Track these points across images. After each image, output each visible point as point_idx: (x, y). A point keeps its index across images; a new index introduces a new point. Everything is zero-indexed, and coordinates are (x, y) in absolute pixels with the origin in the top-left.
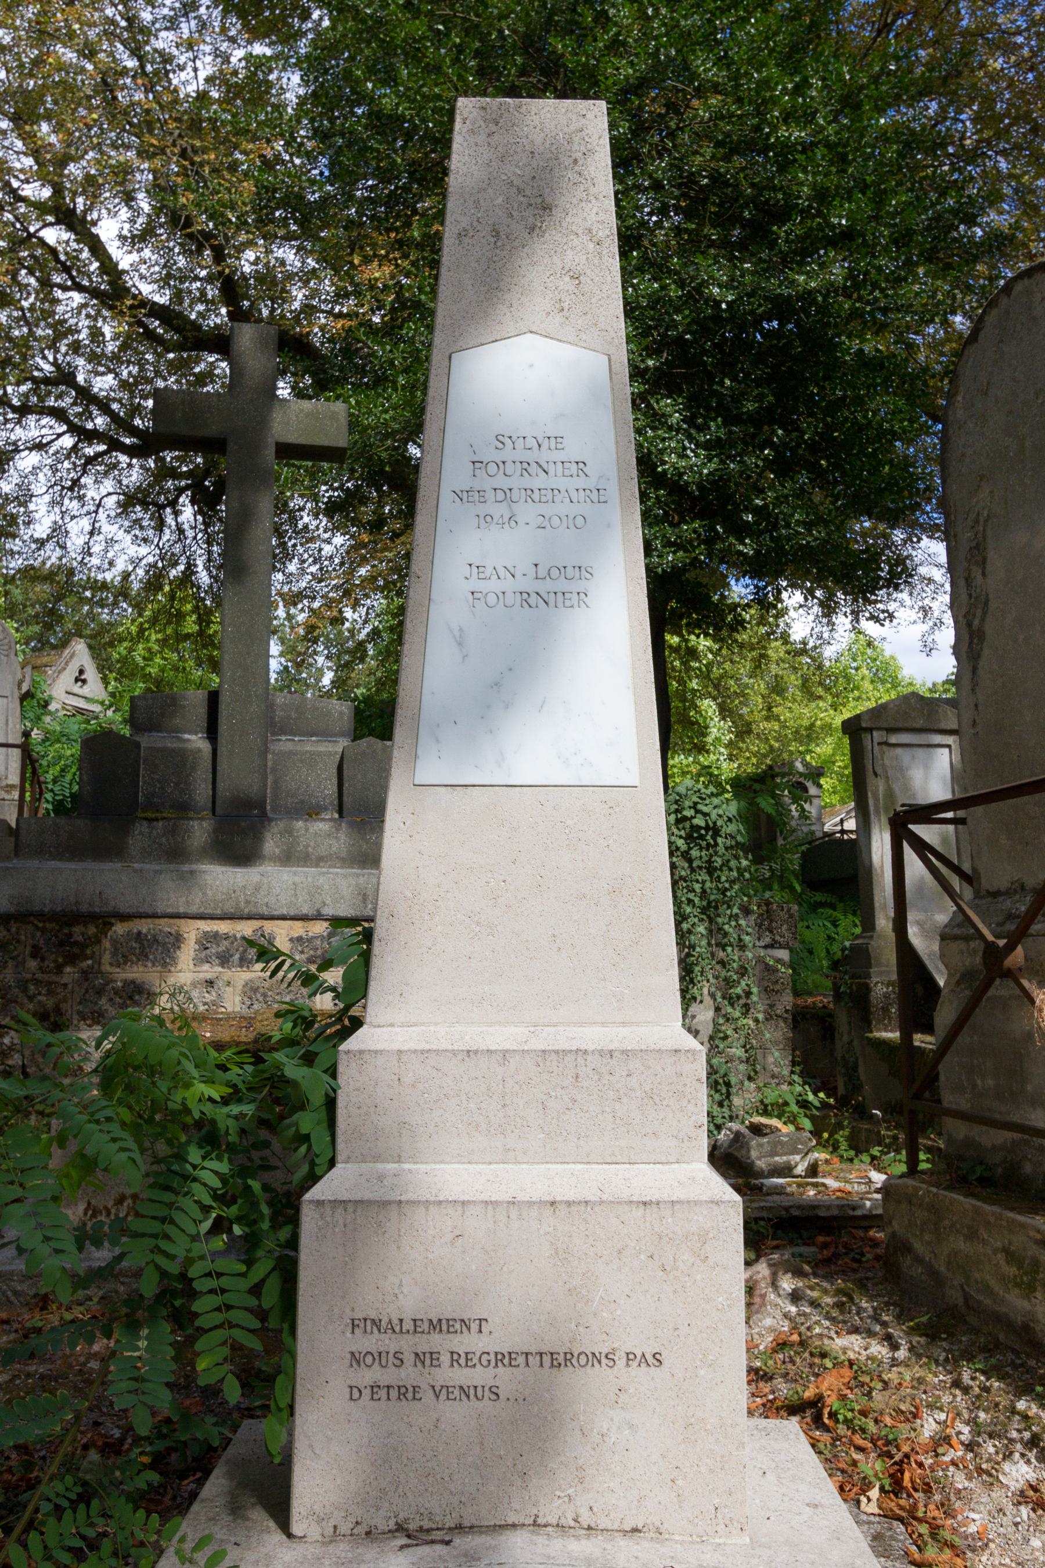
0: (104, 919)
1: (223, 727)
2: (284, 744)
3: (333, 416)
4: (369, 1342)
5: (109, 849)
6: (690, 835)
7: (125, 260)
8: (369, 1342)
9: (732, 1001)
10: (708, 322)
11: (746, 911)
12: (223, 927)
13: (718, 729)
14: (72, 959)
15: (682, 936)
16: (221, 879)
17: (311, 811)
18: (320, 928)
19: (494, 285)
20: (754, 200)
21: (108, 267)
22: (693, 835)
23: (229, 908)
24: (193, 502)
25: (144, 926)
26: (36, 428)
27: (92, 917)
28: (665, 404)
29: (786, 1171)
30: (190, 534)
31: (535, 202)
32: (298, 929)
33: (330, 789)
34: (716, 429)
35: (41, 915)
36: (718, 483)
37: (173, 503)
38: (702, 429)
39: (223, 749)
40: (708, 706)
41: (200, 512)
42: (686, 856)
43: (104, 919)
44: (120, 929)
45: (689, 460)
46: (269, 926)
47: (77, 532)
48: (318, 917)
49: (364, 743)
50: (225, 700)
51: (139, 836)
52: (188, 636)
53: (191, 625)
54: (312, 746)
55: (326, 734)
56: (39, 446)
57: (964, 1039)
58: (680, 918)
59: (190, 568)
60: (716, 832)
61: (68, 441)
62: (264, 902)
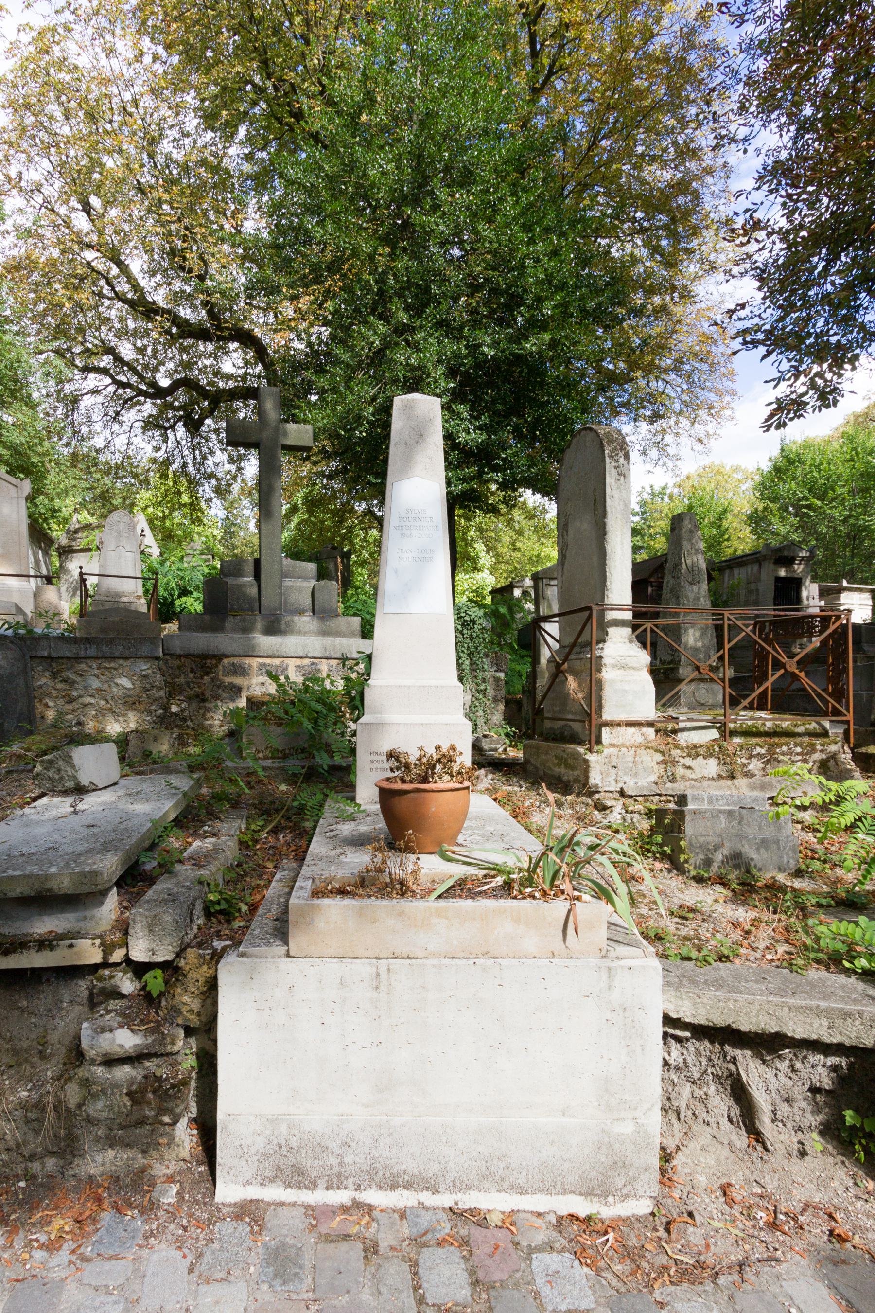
0: (219, 657)
1: (263, 576)
2: (288, 582)
3: (307, 432)
4: (375, 758)
5: (217, 628)
6: (464, 623)
7: (144, 282)
8: (375, 758)
9: (479, 691)
10: (481, 363)
11: (487, 656)
12: (267, 661)
13: (486, 560)
14: (207, 674)
15: (459, 665)
16: (265, 642)
17: (301, 612)
18: (307, 662)
19: (408, 461)
20: (506, 291)
21: (136, 287)
22: (465, 624)
23: (270, 653)
24: (185, 425)
25: (236, 660)
26: (93, 380)
27: (214, 656)
28: (460, 408)
29: (496, 750)
30: (183, 443)
31: (420, 435)
32: (298, 662)
33: (309, 602)
34: (485, 419)
35: (193, 655)
36: (487, 444)
37: (172, 427)
38: (477, 418)
39: (263, 585)
40: (480, 547)
41: (188, 430)
42: (461, 633)
43: (219, 657)
44: (226, 661)
45: (471, 436)
46: (286, 661)
47: (120, 442)
48: (307, 657)
49: (323, 582)
50: (263, 563)
51: (230, 622)
52: (185, 505)
53: (185, 499)
54: (300, 583)
55: (305, 578)
56: (95, 392)
57: (551, 695)
58: (459, 658)
59: (185, 465)
60: (474, 622)
61: (112, 389)
62: (285, 651)
